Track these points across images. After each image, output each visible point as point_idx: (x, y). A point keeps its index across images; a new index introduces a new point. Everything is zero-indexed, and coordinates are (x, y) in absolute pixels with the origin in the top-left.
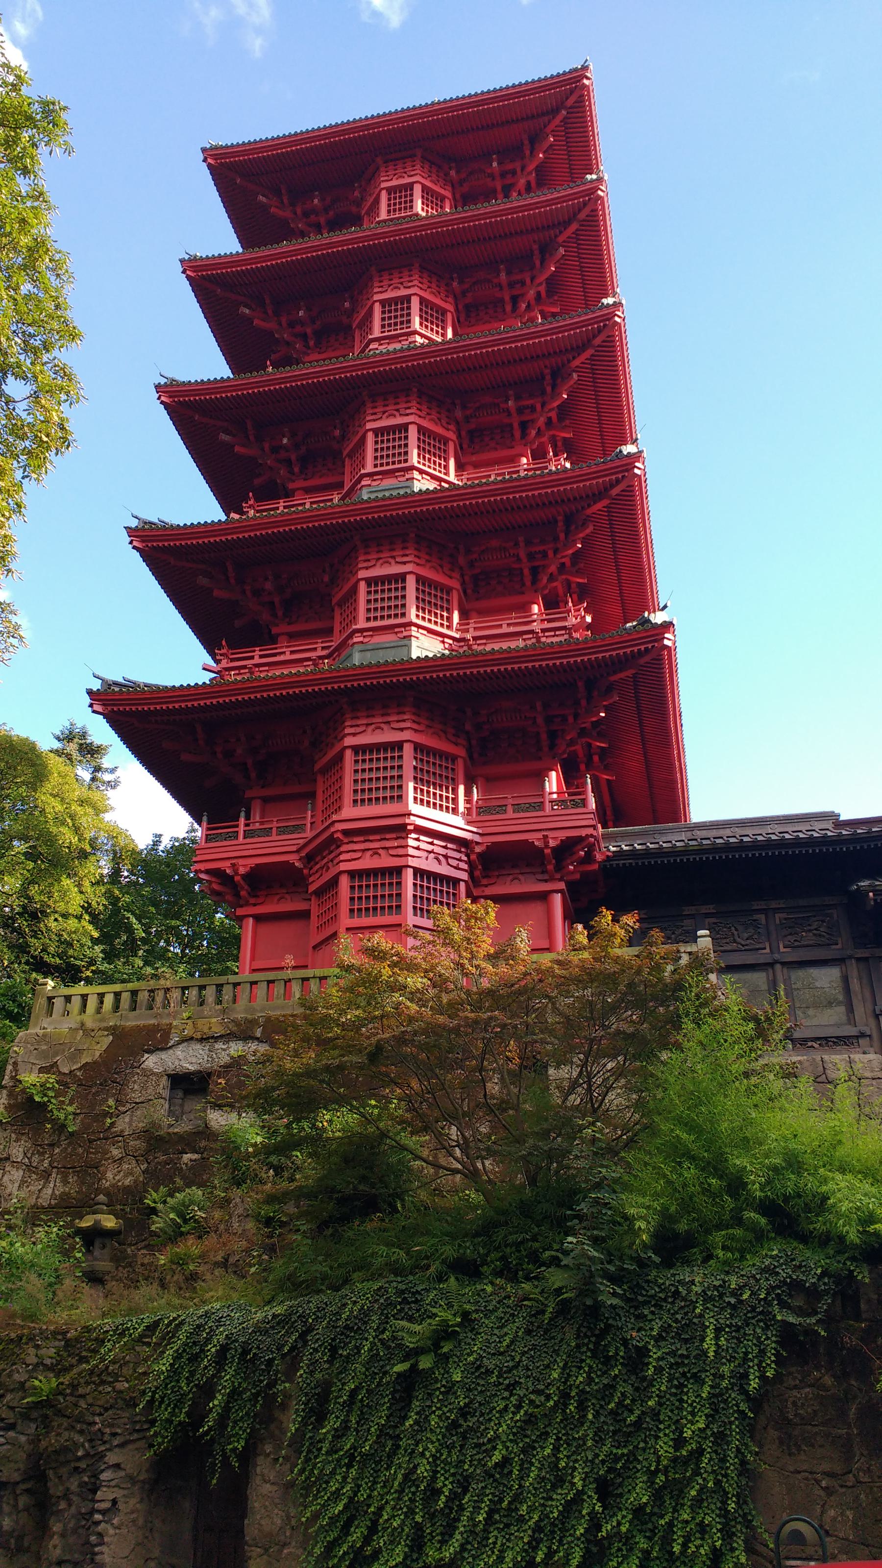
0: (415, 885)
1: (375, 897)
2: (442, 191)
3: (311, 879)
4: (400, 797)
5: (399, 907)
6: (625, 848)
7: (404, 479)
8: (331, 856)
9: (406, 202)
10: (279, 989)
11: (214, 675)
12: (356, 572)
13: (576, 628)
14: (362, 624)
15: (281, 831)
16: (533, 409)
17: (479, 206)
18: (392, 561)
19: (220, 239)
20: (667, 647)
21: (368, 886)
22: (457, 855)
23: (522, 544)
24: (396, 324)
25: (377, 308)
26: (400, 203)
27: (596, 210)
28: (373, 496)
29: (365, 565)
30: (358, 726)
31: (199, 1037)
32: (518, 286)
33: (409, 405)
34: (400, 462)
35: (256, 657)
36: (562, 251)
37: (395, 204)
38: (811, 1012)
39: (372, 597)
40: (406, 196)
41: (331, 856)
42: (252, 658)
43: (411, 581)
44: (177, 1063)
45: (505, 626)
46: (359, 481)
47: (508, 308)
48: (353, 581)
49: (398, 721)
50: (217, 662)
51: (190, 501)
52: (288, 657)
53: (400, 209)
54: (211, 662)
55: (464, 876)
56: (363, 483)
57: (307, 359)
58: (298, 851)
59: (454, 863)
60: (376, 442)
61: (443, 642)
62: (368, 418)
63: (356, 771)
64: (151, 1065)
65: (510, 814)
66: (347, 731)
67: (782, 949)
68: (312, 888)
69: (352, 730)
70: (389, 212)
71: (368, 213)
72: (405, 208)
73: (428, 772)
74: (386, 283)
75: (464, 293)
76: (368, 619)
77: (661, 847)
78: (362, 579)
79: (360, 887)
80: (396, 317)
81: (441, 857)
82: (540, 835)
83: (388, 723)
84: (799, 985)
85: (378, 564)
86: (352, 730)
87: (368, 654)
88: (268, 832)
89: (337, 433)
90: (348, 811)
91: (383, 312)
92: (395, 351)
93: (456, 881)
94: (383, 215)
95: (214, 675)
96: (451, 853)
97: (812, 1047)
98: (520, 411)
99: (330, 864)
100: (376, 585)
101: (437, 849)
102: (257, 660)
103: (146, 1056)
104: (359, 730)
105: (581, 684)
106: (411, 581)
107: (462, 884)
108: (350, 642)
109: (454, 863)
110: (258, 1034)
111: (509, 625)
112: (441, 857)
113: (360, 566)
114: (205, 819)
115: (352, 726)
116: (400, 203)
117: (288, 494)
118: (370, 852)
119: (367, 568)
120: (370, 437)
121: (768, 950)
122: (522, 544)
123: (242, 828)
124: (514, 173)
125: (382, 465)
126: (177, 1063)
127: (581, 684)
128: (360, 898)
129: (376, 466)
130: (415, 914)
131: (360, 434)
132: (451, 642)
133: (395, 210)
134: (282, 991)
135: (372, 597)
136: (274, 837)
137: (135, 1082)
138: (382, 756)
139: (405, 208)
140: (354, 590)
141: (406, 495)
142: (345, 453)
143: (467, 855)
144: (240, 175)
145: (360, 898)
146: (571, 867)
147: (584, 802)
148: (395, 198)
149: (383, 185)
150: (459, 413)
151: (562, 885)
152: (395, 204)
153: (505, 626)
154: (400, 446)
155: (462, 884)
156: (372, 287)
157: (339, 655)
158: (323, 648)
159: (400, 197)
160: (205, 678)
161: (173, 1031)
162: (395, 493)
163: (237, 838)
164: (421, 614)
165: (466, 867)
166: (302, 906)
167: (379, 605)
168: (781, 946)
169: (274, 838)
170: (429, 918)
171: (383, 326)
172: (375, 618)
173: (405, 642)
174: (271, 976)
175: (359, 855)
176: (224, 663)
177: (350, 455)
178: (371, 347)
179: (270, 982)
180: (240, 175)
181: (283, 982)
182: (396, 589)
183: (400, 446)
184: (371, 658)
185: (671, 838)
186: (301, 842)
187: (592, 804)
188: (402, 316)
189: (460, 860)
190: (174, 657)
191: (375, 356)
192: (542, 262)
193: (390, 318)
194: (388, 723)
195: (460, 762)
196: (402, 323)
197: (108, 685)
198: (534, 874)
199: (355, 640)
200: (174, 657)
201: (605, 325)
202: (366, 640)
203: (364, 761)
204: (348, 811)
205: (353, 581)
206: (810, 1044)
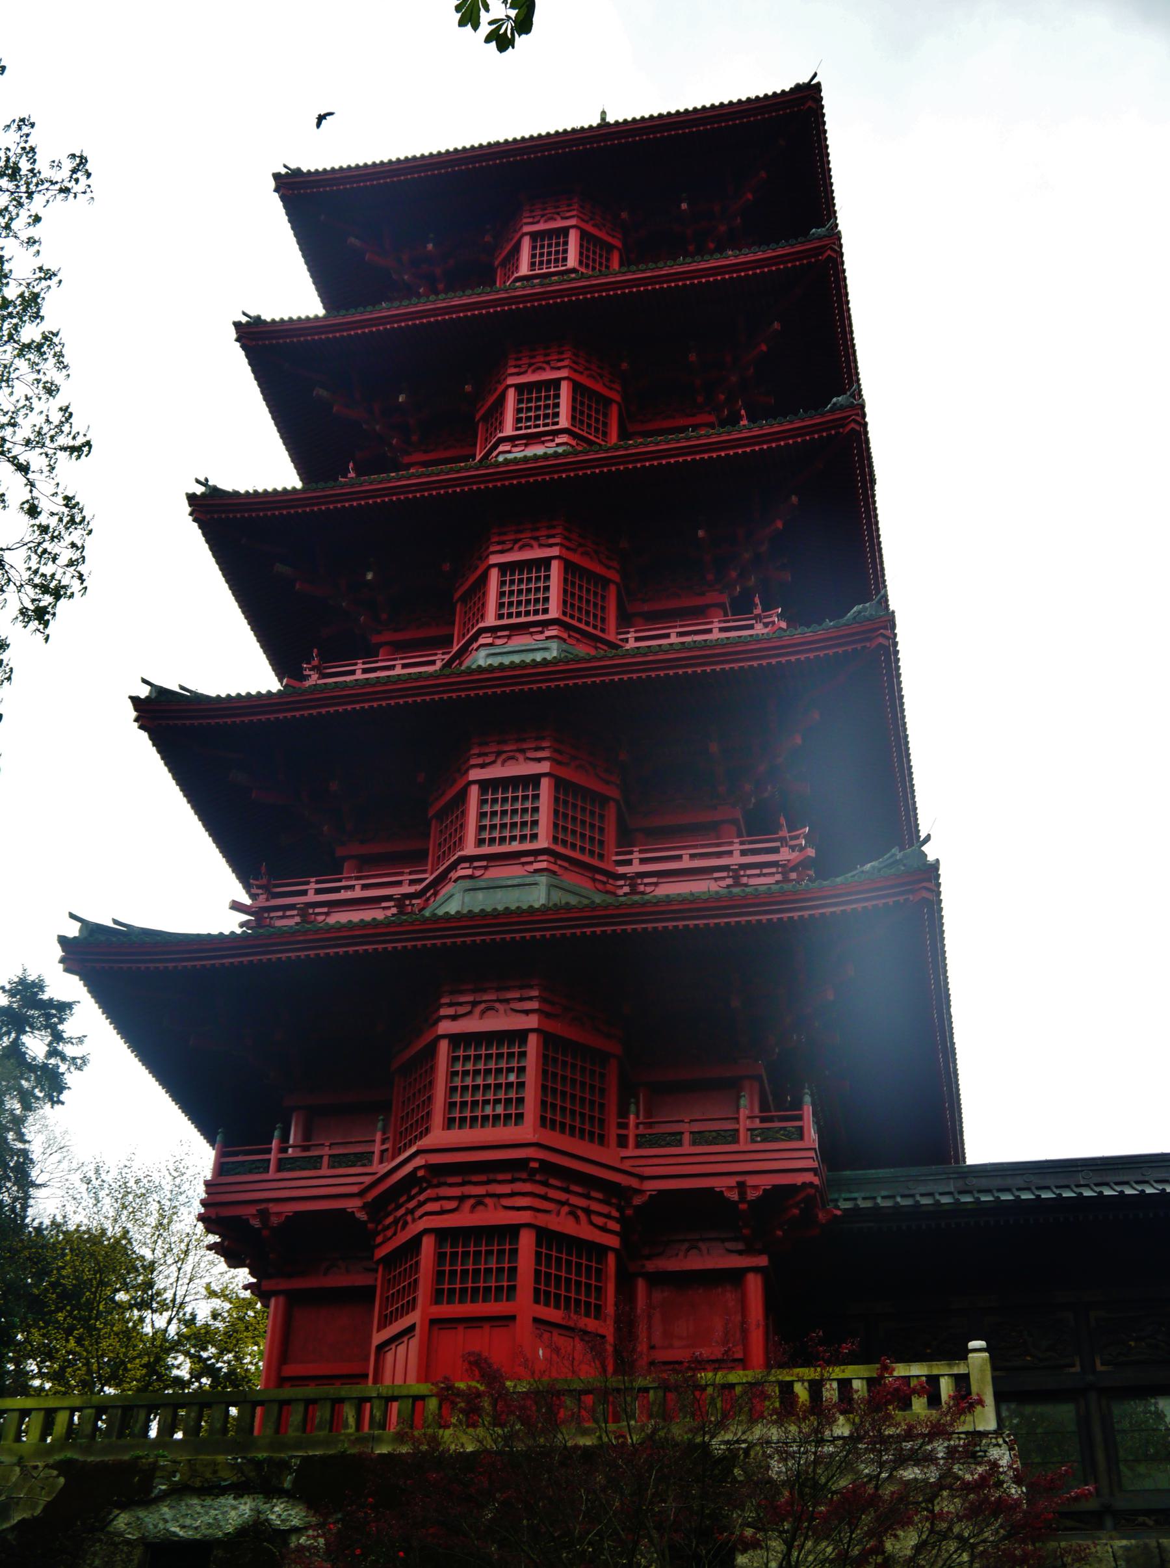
1: (476, 1272)
2: (610, 240)
3: (379, 1239)
5: (512, 1289)
6: (863, 1204)
7: (542, 637)
8: (411, 1205)
9: (557, 252)
10: (322, 1413)
11: (245, 918)
12: (467, 771)
15: (337, 1161)
17: (660, 265)
19: (294, 296)
21: (466, 1254)
22: (604, 1209)
24: (537, 418)
25: (511, 395)
26: (549, 254)
28: (495, 661)
29: (480, 761)
30: (461, 1004)
31: (198, 1484)
33: (553, 532)
34: (536, 612)
35: (311, 893)
37: (542, 255)
38: (1142, 1469)
40: (558, 244)
41: (411, 1205)
42: (305, 893)
43: (565, 388)
44: (161, 1526)
45: (686, 858)
46: (475, 638)
48: (461, 783)
49: (521, 1000)
50: (253, 896)
51: (232, 662)
52: (358, 893)
53: (549, 262)
54: (246, 900)
55: (614, 1242)
56: (481, 641)
57: (406, 460)
58: (361, 1194)
59: (599, 1221)
60: (503, 583)
61: (594, 880)
62: (492, 549)
64: (122, 1526)
65: (687, 1148)
66: (444, 1012)
67: (1100, 1368)
68: (381, 1253)
69: (450, 1011)
70: (533, 264)
71: (503, 264)
72: (556, 260)
73: (564, 1078)
74: (525, 361)
76: (480, 842)
77: (917, 1205)
78: (526, 234)
79: (454, 1255)
80: (538, 408)
81: (580, 1213)
82: (732, 1181)
84: (1126, 1425)
85: (499, 762)
86: (450, 1011)
87: (480, 895)
88: (315, 1163)
89: (447, 567)
90: (438, 1136)
91: (520, 401)
92: (536, 458)
93: (601, 1251)
94: (524, 270)
95: (245, 918)
96: (595, 1206)
97: (1144, 1524)
99: (409, 1218)
100: (530, 392)
101: (574, 1200)
102: (311, 897)
103: (116, 1512)
104: (462, 1010)
107: (611, 1258)
108: (454, 875)
109: (599, 1221)
110: (287, 1485)
111: (692, 856)
112: (580, 1213)
113: (472, 762)
114: (218, 1138)
115: (450, 1005)
116: (549, 254)
117: (369, 652)
118: (472, 1201)
119: (483, 766)
120: (494, 574)
121: (1077, 1369)
123: (273, 1157)
125: (510, 615)
126: (161, 1526)
128: (453, 1273)
129: (480, 842)
130: (537, 1301)
131: (479, 572)
133: (541, 263)
134: (327, 1416)
135: (487, 808)
136: (325, 1171)
137: (95, 1554)
138: (505, 1050)
139: (556, 260)
140: (463, 795)
142: (457, 595)
143: (620, 1209)
145: (453, 1273)
146: (779, 1233)
147: (800, 1134)
148: (542, 247)
149: (526, 229)
151: (763, 1261)
152: (542, 255)
153: (686, 858)
154: (537, 589)
155: (611, 1258)
157: (435, 894)
158: (412, 882)
159: (550, 246)
160: (231, 923)
161: (158, 1474)
162: (528, 658)
163: (267, 1170)
164: (561, 836)
165: (616, 1227)
166: (360, 1280)
168: (1098, 1362)
169: (325, 1171)
170: (557, 1307)
171: (519, 420)
172: (492, 841)
174: (310, 1391)
175: (453, 1205)
176: (262, 901)
177: (465, 599)
178: (501, 448)
179: (310, 1402)
181: (328, 1405)
183: (537, 589)
184: (480, 902)
185: (932, 1193)
186: (367, 1180)
187: (812, 1135)
188: (547, 407)
189: (608, 1216)
190: (194, 890)
191: (507, 462)
193: (529, 409)
194: (507, 1001)
195: (613, 589)
196: (546, 416)
197: (91, 930)
198: (723, 1241)
200: (194, 890)
202: (478, 873)
204: (438, 1136)
205: (461, 783)
206: (1141, 1519)
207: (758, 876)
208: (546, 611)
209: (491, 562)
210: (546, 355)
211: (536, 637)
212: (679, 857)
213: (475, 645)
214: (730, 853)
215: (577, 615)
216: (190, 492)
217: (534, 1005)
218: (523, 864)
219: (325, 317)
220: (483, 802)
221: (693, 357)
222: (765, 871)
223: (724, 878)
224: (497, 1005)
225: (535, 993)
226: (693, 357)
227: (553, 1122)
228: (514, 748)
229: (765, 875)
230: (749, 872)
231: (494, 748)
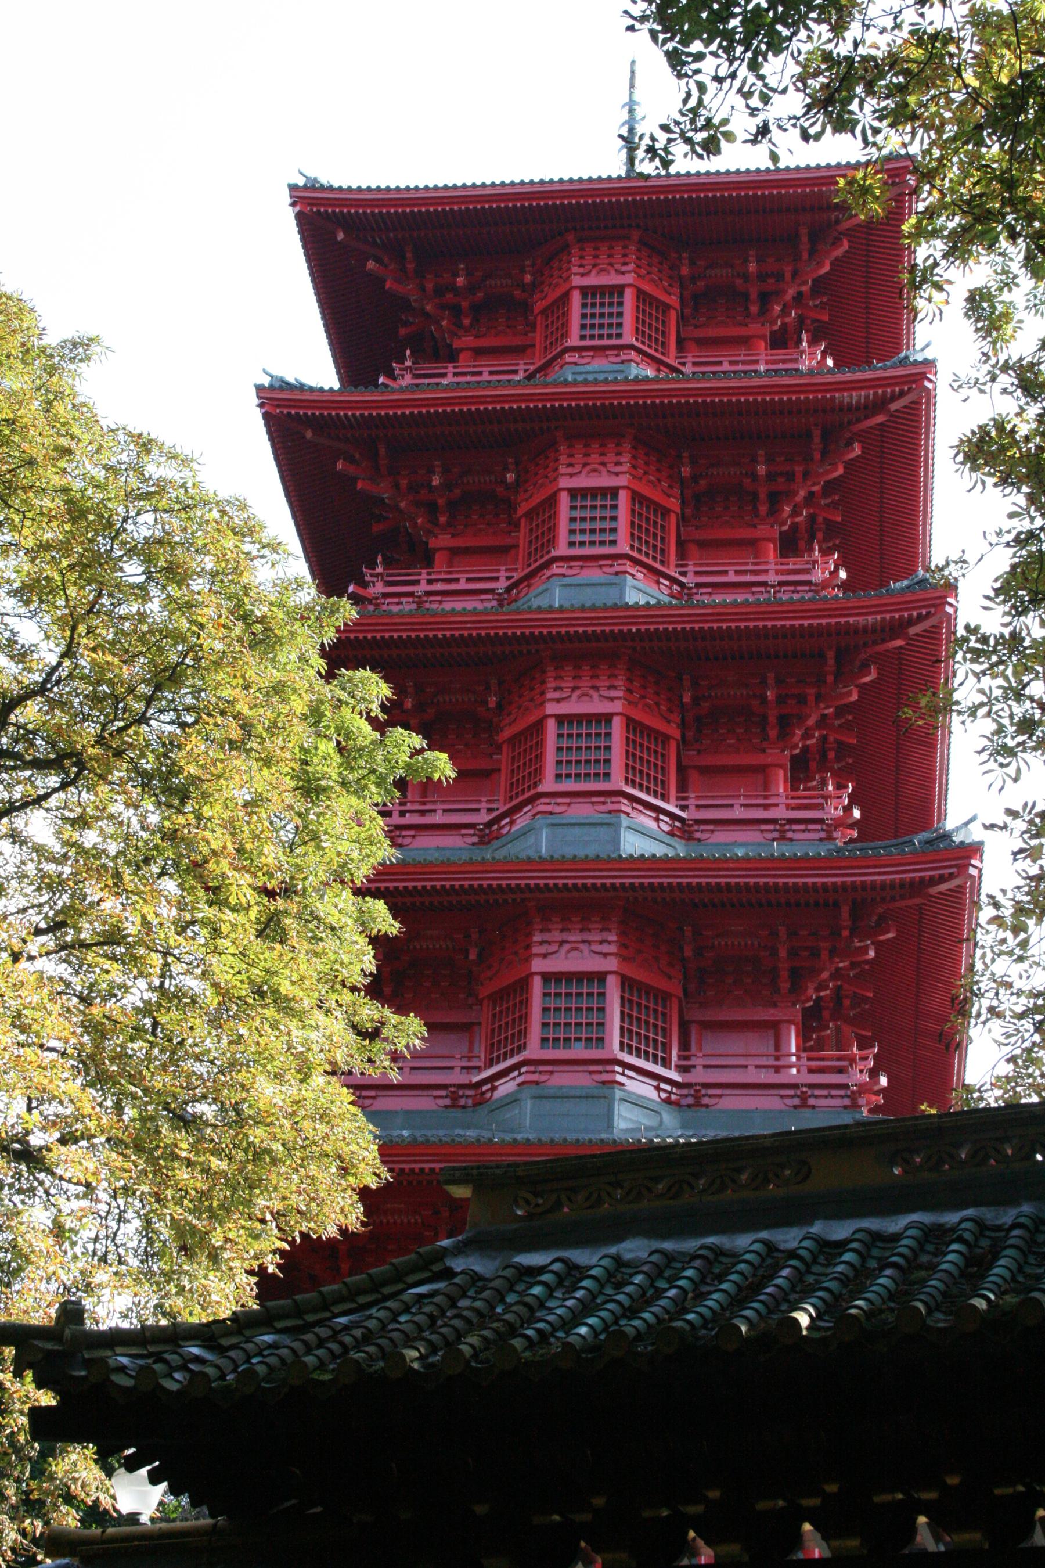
0: (622, 1028)
4: (601, 1040)
7: (618, 359)
13: (824, 585)
14: (574, 341)
16: (779, 277)
18: (595, 695)
20: (972, 876)
23: (771, 681)
27: (919, 403)
28: (580, 378)
32: (771, 281)
36: (857, 450)
39: (588, 311)
43: (629, 295)
46: (548, 565)
47: (763, 509)
49: (601, 942)
63: (573, 520)
69: (542, 949)
75: (695, 478)
76: (583, 337)
78: (576, 287)
83: (589, 942)
85: (584, 472)
98: (781, 699)
100: (594, 295)
105: (830, 655)
106: (629, 295)
122: (771, 681)
124: (790, 477)
127: (830, 655)
129: (583, 337)
132: (668, 1088)
135: (588, 311)
141: (615, 607)
144: (362, 248)
150: (686, 471)
156: (530, 935)
167: (596, 321)
173: (605, 1091)
180: (362, 248)
182: (611, 304)
192: (824, 453)
194: (589, 942)
199: (568, 360)
201: (928, 613)
203: (570, 736)
207: (826, 1097)
208: (619, 336)
209: (549, 712)
210: (602, 454)
211: (605, 569)
212: (726, 572)
213: (548, 573)
214: (766, 571)
215: (644, 549)
216: (259, 382)
217: (613, 949)
218: (591, 1073)
219: (340, 392)
220: (584, 305)
221: (752, 267)
222: (811, 827)
223: (792, 1097)
224: (581, 946)
225: (613, 937)
226: (752, 267)
227: (630, 1046)
228: (579, 938)
229: (832, 1097)
230: (794, 827)
231: (557, 936)
